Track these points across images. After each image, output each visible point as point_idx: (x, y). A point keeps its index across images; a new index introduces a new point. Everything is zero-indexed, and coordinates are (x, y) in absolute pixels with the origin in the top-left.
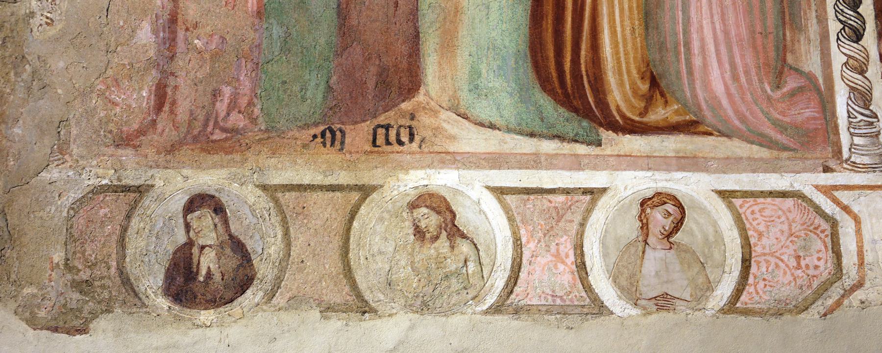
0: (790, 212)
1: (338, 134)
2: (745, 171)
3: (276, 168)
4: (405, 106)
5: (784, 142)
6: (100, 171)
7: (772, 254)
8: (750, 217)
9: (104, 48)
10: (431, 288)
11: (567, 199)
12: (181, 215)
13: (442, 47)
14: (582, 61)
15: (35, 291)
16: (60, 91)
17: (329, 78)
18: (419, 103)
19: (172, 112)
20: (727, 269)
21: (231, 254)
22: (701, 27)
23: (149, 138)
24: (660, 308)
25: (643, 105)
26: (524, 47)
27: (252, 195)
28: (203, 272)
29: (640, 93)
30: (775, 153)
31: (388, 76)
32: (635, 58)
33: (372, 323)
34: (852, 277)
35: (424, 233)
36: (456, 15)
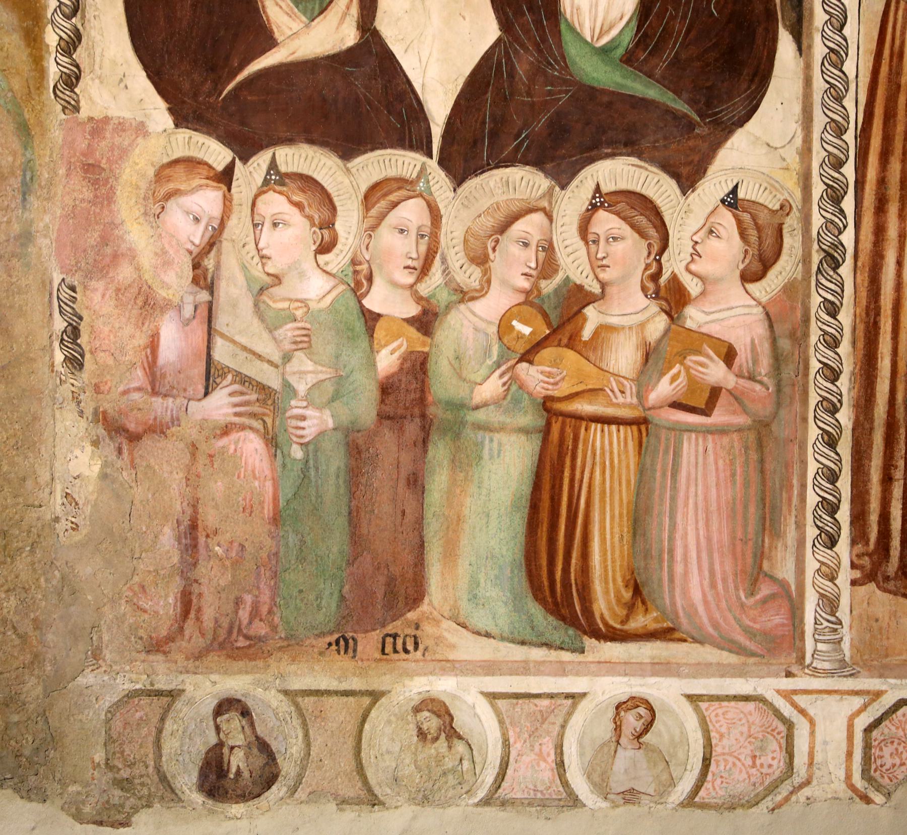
0: (751, 714)
1: (351, 642)
2: (713, 676)
3: (296, 674)
4: (411, 615)
5: (753, 648)
6: (134, 676)
7: (730, 754)
8: (714, 719)
9: (129, 555)
10: (431, 783)
11: (551, 703)
12: (211, 718)
13: (445, 557)
14: (572, 570)
15: (80, 789)
16: (89, 597)
17: (342, 587)
18: (423, 613)
19: (198, 619)
20: (689, 767)
21: (258, 754)
22: (686, 534)
23: (178, 644)
24: (627, 802)
25: (625, 612)
26: (520, 556)
27: (274, 699)
28: (233, 770)
29: (624, 601)
30: (743, 659)
31: (395, 586)
32: (621, 566)
33: (380, 814)
34: (801, 775)
35: (426, 735)
36: (458, 524)
